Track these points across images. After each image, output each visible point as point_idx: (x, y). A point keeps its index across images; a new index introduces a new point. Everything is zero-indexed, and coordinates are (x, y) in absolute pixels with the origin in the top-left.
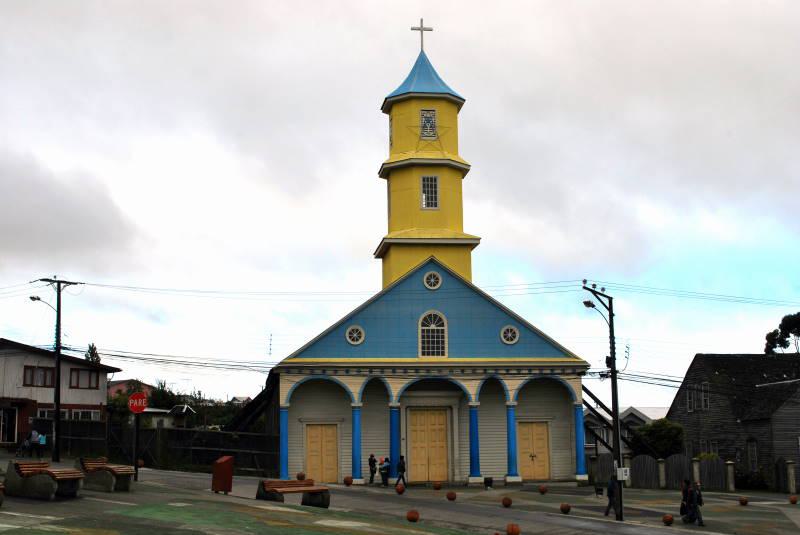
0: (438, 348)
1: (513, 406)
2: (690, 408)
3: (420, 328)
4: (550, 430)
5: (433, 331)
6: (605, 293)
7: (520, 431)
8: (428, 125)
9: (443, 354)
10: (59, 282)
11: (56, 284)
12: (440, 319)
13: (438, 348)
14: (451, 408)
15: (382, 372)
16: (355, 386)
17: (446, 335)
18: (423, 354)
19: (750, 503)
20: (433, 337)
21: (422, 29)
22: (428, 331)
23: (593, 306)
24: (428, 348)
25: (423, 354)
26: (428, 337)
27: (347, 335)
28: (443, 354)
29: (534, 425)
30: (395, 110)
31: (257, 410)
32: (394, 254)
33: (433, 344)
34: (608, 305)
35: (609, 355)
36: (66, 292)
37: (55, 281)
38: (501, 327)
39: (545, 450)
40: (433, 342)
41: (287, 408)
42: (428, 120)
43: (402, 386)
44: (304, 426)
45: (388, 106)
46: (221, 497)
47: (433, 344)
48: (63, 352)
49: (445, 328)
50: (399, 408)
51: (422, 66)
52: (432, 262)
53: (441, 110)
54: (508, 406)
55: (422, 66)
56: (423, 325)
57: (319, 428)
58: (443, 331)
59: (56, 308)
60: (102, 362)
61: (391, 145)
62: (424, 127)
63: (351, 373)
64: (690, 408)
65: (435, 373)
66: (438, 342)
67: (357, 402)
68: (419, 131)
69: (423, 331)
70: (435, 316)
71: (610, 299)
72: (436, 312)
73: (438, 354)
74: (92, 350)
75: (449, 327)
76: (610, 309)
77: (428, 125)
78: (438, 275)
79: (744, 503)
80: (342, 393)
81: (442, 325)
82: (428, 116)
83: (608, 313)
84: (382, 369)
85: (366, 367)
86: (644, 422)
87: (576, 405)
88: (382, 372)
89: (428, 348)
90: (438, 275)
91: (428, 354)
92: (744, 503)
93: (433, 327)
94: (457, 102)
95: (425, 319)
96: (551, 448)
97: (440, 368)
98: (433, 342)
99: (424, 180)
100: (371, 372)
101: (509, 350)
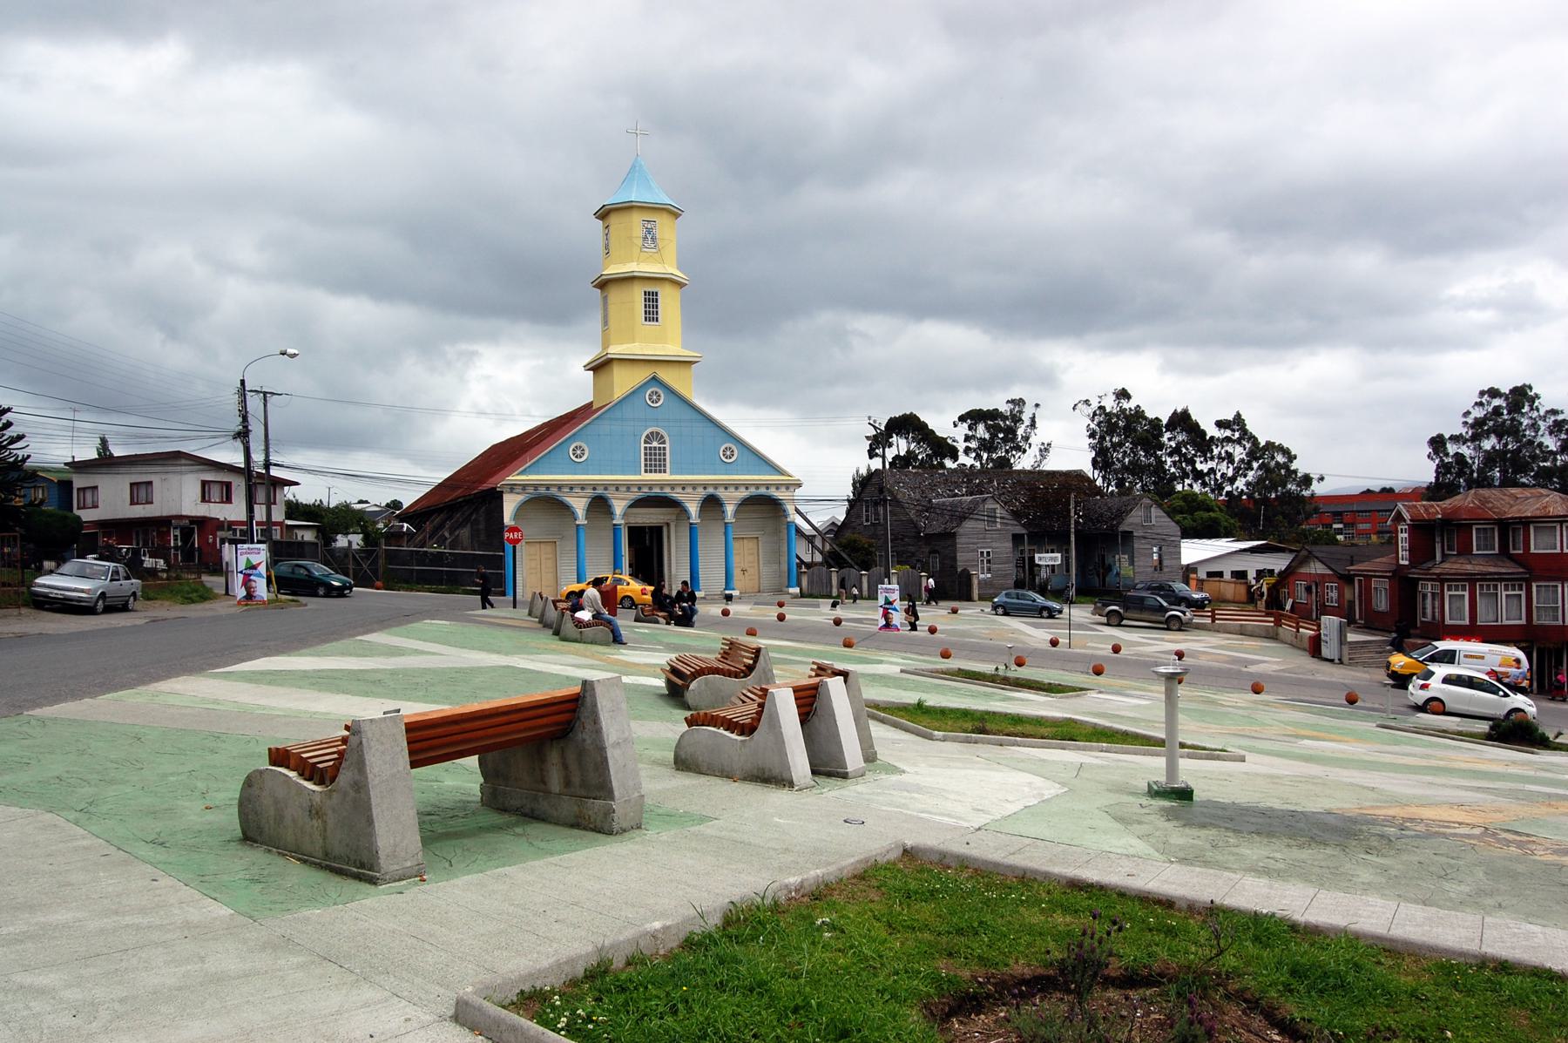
0: (660, 466)
2: (867, 521)
3: (643, 445)
4: (760, 544)
5: (655, 448)
7: (736, 546)
8: (649, 237)
9: (665, 472)
10: (265, 393)
11: (262, 395)
12: (662, 437)
14: (668, 525)
16: (579, 505)
17: (668, 452)
18: (646, 471)
19: (959, 612)
20: (655, 454)
22: (650, 448)
24: (651, 465)
25: (646, 471)
26: (651, 454)
27: (723, 448)
28: (665, 472)
30: (614, 220)
31: (1509, 785)
33: (655, 461)
36: (272, 400)
37: (261, 392)
38: (722, 445)
39: (756, 564)
40: (655, 460)
42: (649, 231)
43: (624, 504)
47: (655, 461)
48: (274, 472)
49: (667, 446)
52: (655, 380)
56: (646, 442)
57: (538, 545)
58: (664, 448)
59: (263, 421)
60: (115, 455)
62: (645, 238)
63: (515, 491)
64: (867, 521)
65: (656, 490)
67: (581, 519)
68: (640, 242)
69: (646, 448)
70: (658, 433)
73: (660, 472)
74: (868, 438)
77: (649, 237)
79: (955, 611)
80: (565, 508)
81: (664, 443)
82: (649, 227)
83: (275, 396)
84: (716, 486)
85: (519, 485)
87: (788, 522)
89: (651, 465)
92: (955, 611)
93: (655, 444)
95: (647, 436)
96: (761, 562)
97: (662, 486)
98: (655, 460)
99: (645, 295)
101: (728, 468)
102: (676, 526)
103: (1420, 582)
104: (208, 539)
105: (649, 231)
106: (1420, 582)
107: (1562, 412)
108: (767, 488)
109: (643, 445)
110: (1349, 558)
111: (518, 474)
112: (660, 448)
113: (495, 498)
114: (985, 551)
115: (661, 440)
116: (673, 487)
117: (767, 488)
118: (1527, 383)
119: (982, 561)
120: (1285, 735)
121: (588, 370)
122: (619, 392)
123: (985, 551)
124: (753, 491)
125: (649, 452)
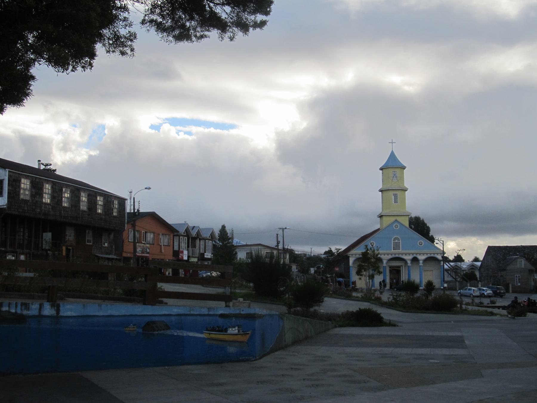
0: (398, 248)
1: (422, 266)
3: (392, 241)
5: (396, 242)
6: (441, 240)
9: (400, 250)
11: (282, 229)
12: (399, 239)
13: (398, 248)
14: (402, 266)
15: (402, 255)
18: (394, 250)
21: (392, 143)
22: (395, 242)
23: (438, 244)
25: (394, 250)
29: (429, 271)
32: (384, 218)
34: (442, 243)
35: (168, 304)
36: (285, 230)
41: (352, 266)
42: (395, 175)
44: (423, 271)
45: (381, 169)
46: (383, 272)
49: (400, 241)
50: (386, 266)
51: (392, 156)
52: (396, 220)
53: (398, 171)
54: (420, 266)
55: (392, 156)
56: (393, 241)
58: (400, 242)
61: (383, 182)
66: (398, 246)
69: (393, 242)
71: (443, 241)
72: (397, 237)
73: (398, 250)
75: (402, 241)
76: (443, 244)
77: (395, 176)
78: (398, 225)
81: (399, 241)
83: (442, 245)
84: (416, 254)
86: (461, 269)
88: (402, 255)
90: (398, 225)
91: (395, 250)
93: (396, 241)
94: (404, 168)
95: (394, 239)
97: (399, 254)
100: (413, 255)
102: (405, 267)
103: (15, 254)
104: (10, 261)
105: (395, 175)
106: (15, 254)
107: (72, 71)
108: (434, 255)
109: (392, 241)
110: (169, 245)
111: (354, 251)
112: (398, 242)
113: (348, 258)
114: (518, 275)
115: (399, 239)
116: (402, 254)
117: (434, 255)
118: (95, 62)
119: (517, 279)
120: (299, 369)
121: (378, 217)
122: (385, 225)
123: (518, 275)
124: (393, 256)
125: (395, 243)
